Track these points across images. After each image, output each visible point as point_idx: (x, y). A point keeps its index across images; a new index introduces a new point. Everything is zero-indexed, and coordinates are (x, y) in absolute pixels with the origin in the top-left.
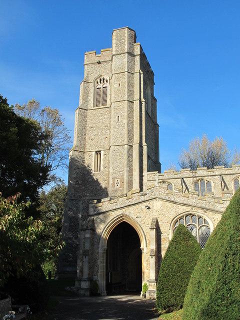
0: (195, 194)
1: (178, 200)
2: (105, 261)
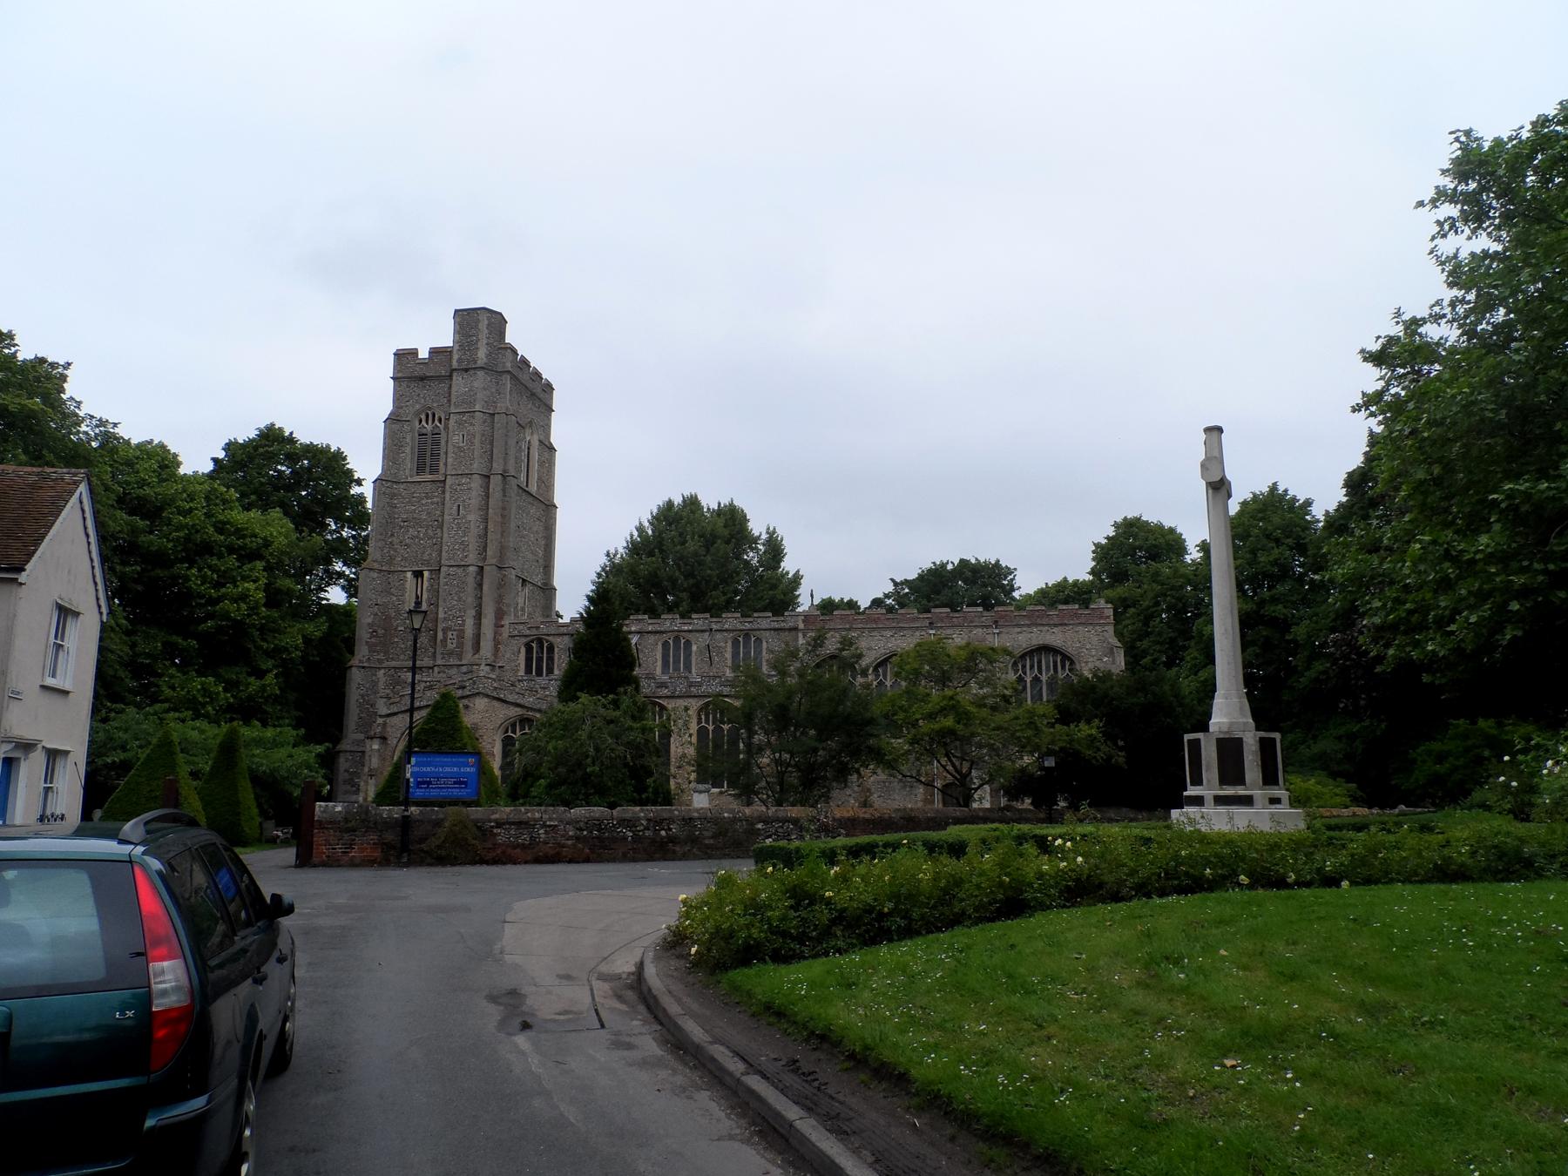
1: (510, 698)
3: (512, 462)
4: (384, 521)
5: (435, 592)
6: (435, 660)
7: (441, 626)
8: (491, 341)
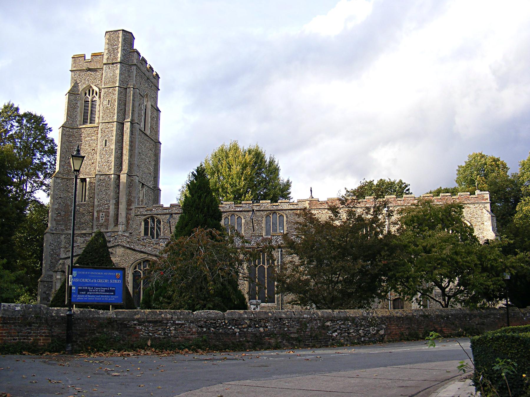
0: (152, 243)
1: (137, 248)
3: (136, 115)
4: (65, 150)
6: (93, 229)
7: (96, 209)
8: (126, 48)
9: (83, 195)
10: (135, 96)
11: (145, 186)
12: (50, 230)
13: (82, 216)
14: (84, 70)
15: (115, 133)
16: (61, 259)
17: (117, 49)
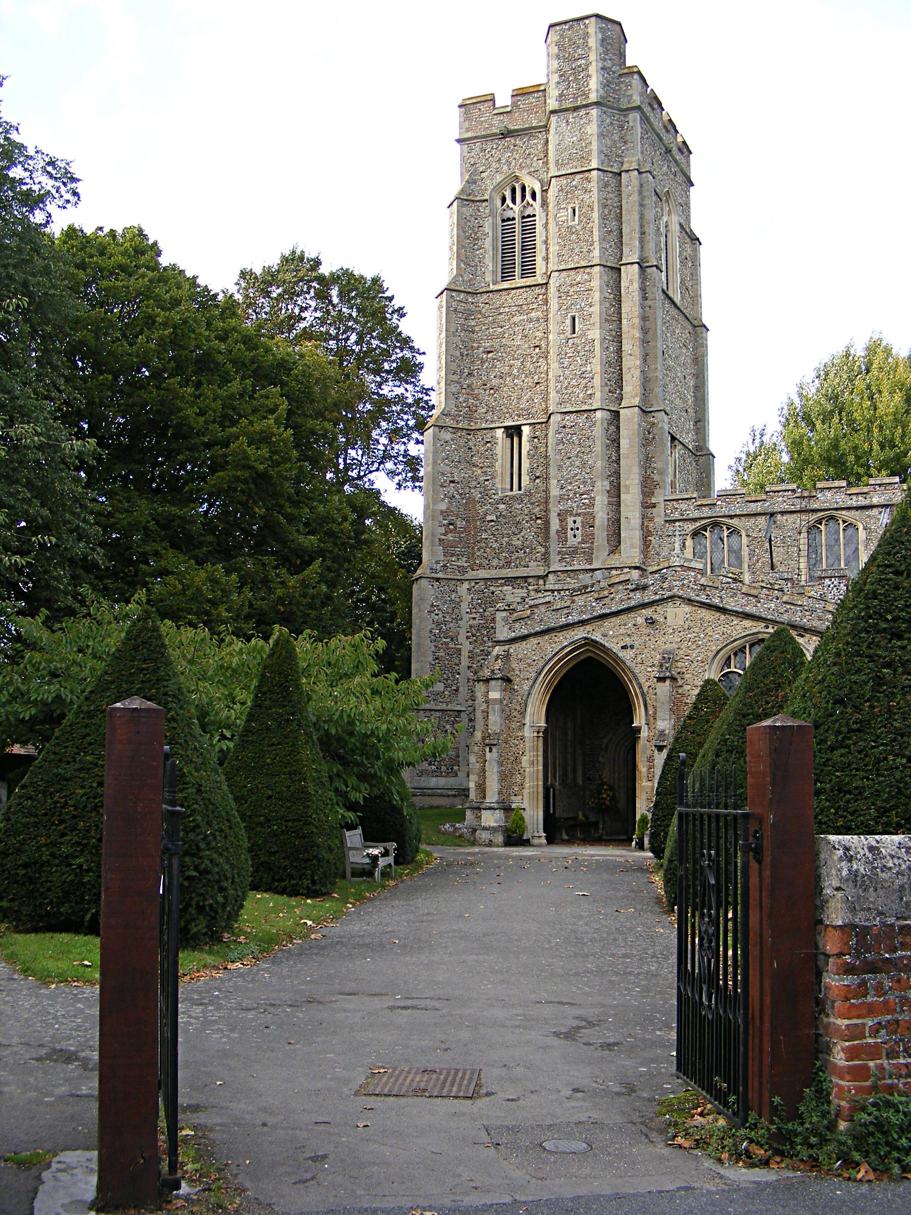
0: (776, 587)
2: (541, 759)
3: (651, 246)
4: (458, 354)
5: (542, 459)
7: (554, 510)
8: (609, 64)
9: (515, 474)
10: (645, 194)
11: (677, 443)
12: (428, 571)
13: (514, 529)
14: (495, 135)
15: (597, 295)
16: (499, 643)
17: (586, 69)
